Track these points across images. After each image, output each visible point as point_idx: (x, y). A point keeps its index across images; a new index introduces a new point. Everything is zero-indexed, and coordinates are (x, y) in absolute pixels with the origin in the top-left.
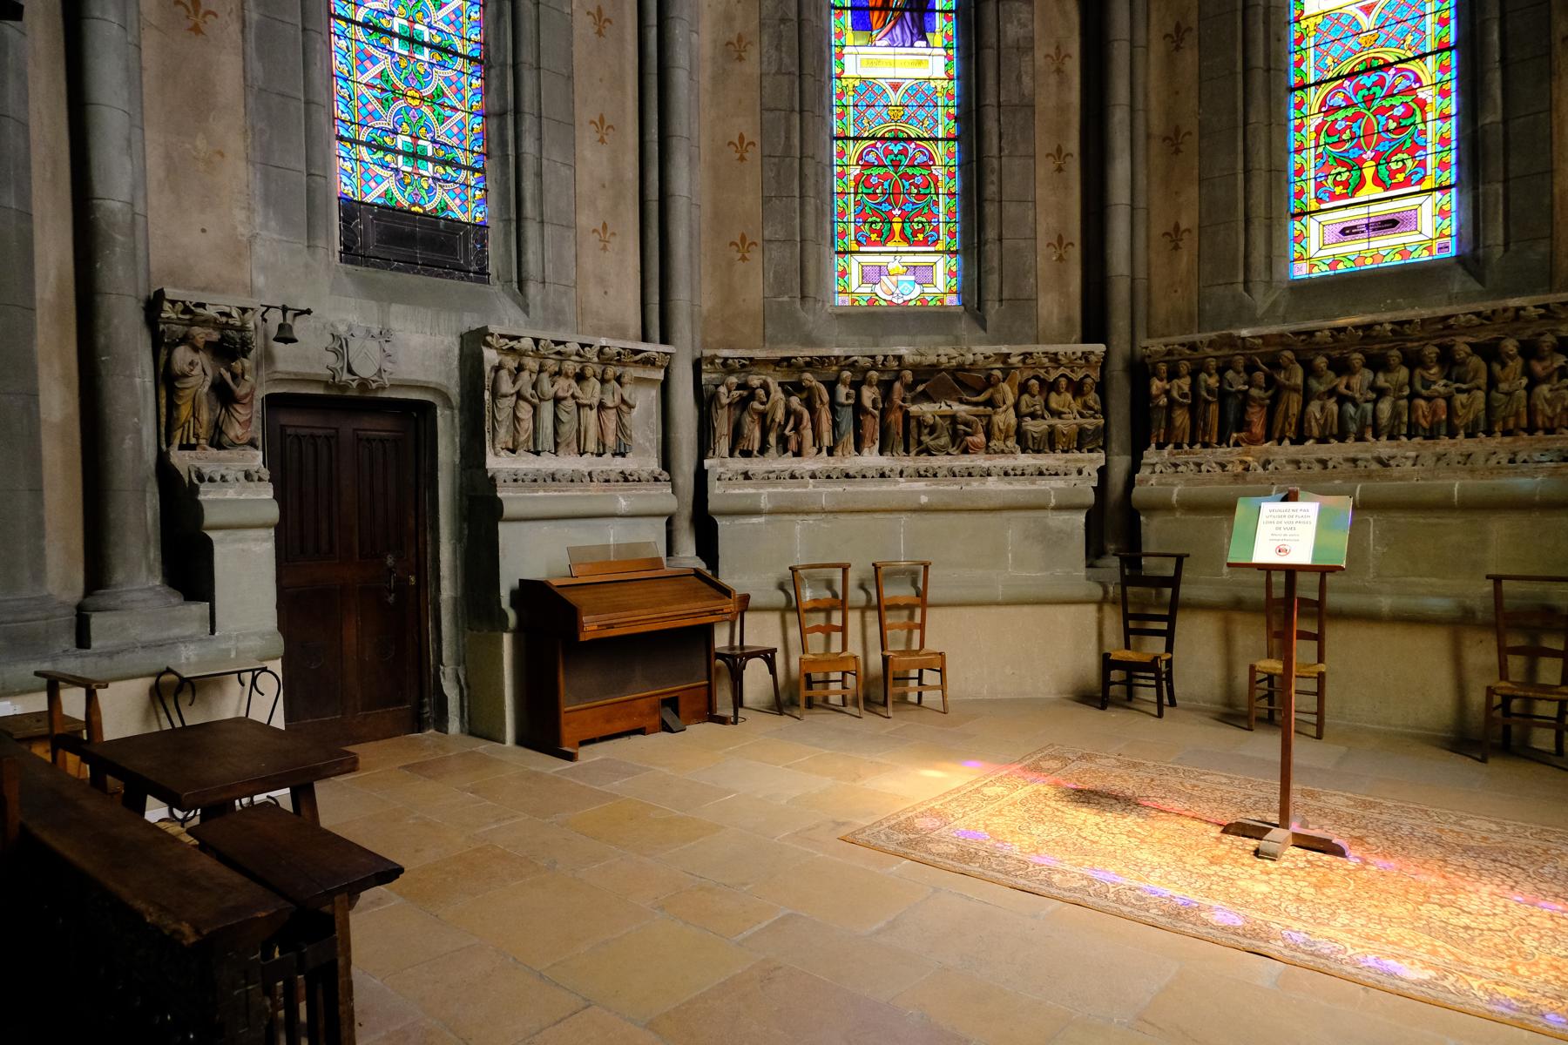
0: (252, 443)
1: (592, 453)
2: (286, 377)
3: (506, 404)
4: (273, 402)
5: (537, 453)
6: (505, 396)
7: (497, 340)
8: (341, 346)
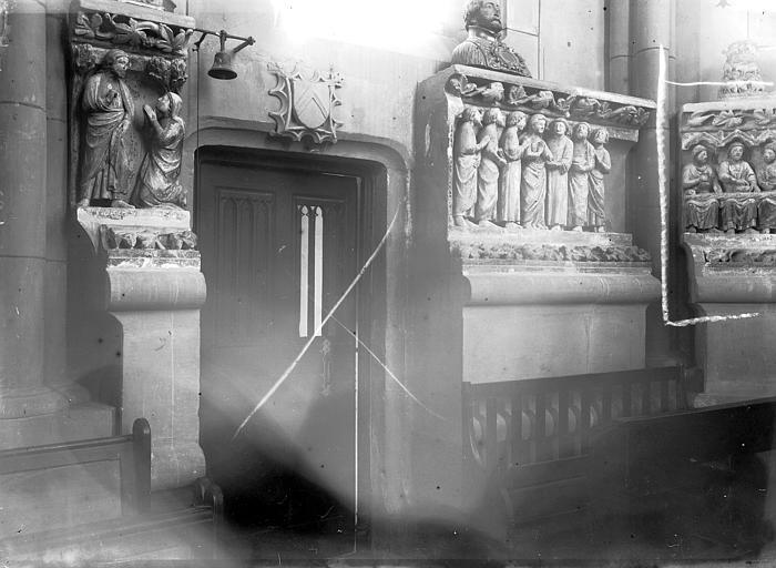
0: (178, 203)
1: (561, 226)
2: (223, 125)
3: (469, 163)
4: (207, 156)
5: (502, 224)
6: (469, 152)
7: (464, 84)
8: (285, 89)
